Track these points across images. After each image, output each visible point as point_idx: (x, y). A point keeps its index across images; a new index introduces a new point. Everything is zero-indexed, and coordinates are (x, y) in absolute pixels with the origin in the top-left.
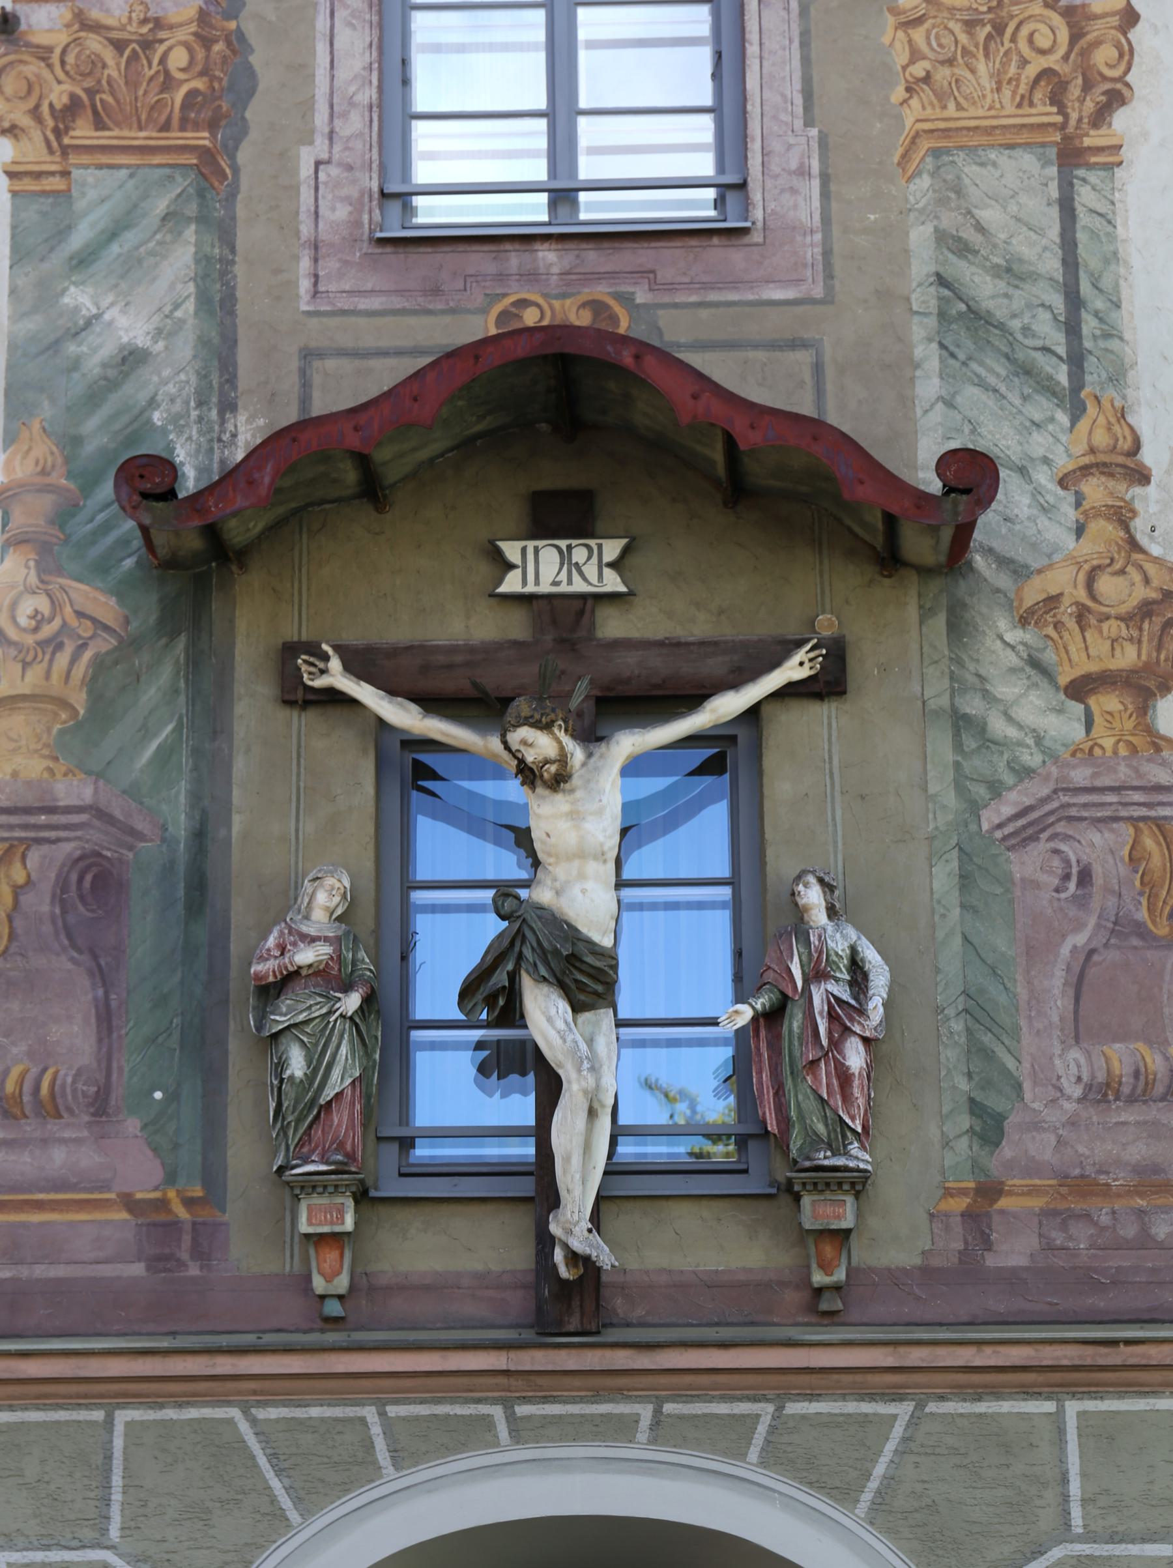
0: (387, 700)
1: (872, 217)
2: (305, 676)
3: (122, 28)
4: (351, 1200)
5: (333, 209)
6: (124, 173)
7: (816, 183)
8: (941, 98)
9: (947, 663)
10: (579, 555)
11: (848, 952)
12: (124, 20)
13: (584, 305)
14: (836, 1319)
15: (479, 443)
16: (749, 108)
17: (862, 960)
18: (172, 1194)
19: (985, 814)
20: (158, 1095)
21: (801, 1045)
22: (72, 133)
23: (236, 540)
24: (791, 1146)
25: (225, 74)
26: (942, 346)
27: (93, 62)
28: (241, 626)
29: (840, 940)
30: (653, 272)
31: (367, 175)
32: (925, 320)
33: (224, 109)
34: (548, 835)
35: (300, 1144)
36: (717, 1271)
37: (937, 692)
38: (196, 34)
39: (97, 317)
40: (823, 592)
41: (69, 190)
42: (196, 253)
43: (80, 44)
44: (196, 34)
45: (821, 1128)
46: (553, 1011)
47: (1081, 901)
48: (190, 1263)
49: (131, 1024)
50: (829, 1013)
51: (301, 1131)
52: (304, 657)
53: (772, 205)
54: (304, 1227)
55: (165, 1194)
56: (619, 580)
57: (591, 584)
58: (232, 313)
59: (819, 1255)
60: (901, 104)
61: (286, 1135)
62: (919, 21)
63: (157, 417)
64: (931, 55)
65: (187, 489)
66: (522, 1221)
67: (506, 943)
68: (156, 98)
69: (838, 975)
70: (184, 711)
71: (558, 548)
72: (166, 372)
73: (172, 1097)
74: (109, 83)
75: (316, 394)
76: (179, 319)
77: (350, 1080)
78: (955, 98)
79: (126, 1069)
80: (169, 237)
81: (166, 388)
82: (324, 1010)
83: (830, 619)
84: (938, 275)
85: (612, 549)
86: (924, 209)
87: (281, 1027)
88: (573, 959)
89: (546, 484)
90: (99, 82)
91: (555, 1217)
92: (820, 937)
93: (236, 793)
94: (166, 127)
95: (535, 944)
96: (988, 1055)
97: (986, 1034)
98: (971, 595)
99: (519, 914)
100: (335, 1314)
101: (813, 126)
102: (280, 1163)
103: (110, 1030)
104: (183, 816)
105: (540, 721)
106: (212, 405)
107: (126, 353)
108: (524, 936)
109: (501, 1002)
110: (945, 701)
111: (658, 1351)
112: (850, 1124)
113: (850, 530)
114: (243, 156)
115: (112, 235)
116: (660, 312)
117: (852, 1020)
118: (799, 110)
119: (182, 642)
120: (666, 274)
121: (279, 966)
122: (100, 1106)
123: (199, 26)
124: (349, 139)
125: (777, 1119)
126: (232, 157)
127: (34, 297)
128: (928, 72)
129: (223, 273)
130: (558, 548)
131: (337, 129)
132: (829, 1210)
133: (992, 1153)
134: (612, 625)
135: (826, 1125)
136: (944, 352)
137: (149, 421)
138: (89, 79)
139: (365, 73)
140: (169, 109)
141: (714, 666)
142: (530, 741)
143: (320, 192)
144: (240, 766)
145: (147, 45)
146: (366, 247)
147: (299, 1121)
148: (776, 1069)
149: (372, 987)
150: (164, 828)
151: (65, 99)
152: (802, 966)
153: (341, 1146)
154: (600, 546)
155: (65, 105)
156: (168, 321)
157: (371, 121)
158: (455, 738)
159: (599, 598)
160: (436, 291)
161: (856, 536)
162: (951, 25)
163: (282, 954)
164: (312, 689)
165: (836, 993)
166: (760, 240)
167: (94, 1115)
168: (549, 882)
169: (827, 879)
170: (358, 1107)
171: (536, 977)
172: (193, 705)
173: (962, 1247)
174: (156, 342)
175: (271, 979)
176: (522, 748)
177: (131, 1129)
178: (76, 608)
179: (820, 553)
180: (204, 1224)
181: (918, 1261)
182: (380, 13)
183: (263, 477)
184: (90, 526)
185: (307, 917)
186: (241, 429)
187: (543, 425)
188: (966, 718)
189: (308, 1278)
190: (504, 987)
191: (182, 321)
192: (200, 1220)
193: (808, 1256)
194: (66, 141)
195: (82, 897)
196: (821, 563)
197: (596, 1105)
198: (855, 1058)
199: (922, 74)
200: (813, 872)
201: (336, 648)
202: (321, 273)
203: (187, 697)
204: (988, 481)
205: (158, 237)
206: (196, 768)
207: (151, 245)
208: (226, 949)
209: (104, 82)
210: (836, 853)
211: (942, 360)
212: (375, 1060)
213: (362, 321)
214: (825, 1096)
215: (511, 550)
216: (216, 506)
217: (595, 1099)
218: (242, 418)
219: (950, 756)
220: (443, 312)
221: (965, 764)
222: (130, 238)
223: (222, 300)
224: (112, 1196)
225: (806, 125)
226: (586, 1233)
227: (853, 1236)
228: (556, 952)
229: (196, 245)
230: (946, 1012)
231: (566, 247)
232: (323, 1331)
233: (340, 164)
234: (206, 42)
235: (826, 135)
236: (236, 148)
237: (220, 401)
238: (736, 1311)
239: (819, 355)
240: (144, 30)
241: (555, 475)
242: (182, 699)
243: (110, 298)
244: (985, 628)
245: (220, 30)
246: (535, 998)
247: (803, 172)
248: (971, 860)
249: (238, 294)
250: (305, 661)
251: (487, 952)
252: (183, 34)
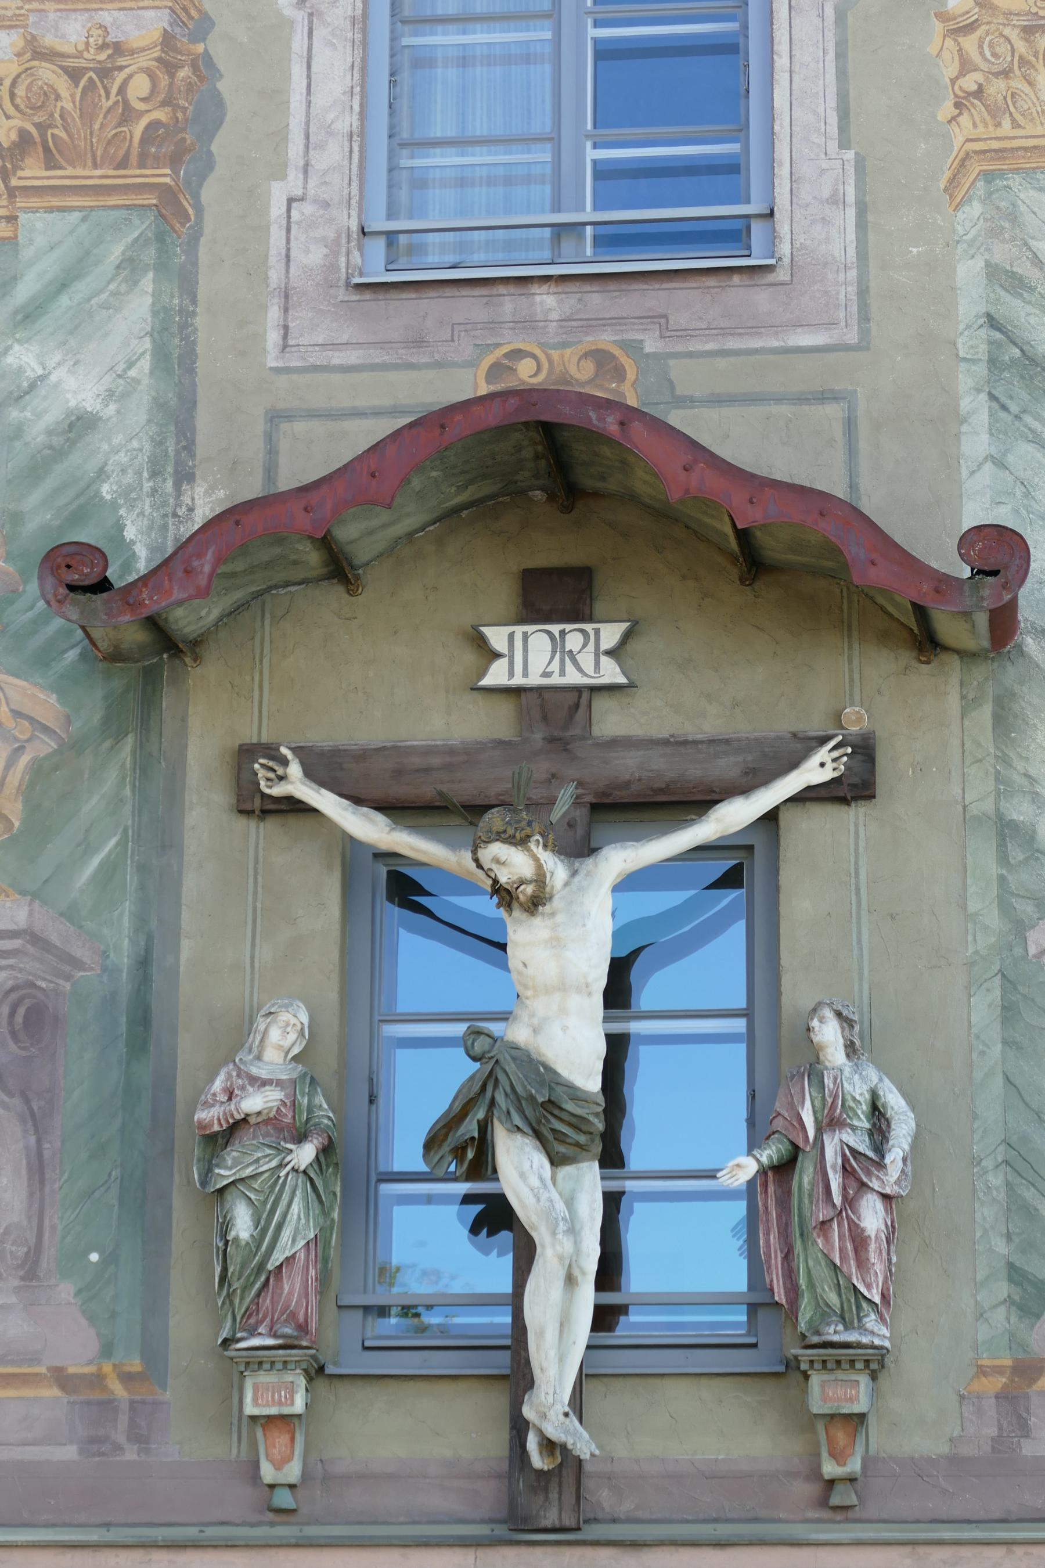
0: (350, 809)
1: (915, 250)
2: (262, 783)
3: (79, 55)
4: (302, 1378)
5: (307, 252)
6: (76, 215)
7: (851, 213)
8: (995, 113)
9: (992, 761)
10: (574, 641)
11: (868, 1096)
12: (81, 47)
13: (586, 355)
14: (850, 1514)
15: (464, 514)
16: (777, 128)
17: (883, 1106)
18: (107, 1368)
19: (1032, 936)
20: (94, 1257)
21: (811, 1202)
22: (20, 173)
23: (187, 630)
24: (800, 1318)
25: (190, 104)
26: (992, 397)
27: (45, 94)
28: (195, 724)
29: (857, 1085)
30: (665, 316)
31: (345, 212)
32: (973, 368)
33: (188, 142)
34: (525, 965)
35: (247, 1314)
36: (716, 1460)
37: (980, 795)
38: (158, 60)
39: (43, 378)
40: (852, 680)
41: (16, 237)
42: (153, 304)
43: (32, 75)
44: (158, 60)
45: (833, 1298)
46: (526, 1166)
48: (127, 1446)
49: (66, 1176)
50: (843, 1167)
51: (248, 1300)
52: (261, 761)
53: (800, 239)
54: (250, 1410)
55: (100, 1369)
56: (618, 670)
57: (586, 675)
58: (191, 371)
59: (830, 1441)
60: (949, 122)
61: (232, 1303)
62: (970, 28)
63: (106, 491)
64: (983, 66)
65: (138, 571)
66: (497, 1400)
67: (476, 1088)
68: (114, 132)
69: (856, 1123)
70: (130, 822)
71: (549, 633)
72: (118, 439)
73: (110, 1259)
74: (62, 116)
75: (283, 460)
76: (133, 379)
77: (303, 1243)
78: (1011, 114)
79: (60, 1228)
80: (123, 288)
81: (117, 457)
82: (274, 1163)
83: (858, 712)
84: (989, 315)
85: (611, 634)
86: (974, 240)
87: (225, 1182)
88: (551, 1106)
89: (541, 560)
90: (52, 115)
91: (530, 1398)
92: (835, 1079)
93: (185, 914)
94: (123, 163)
95: (508, 1089)
96: (1029, 1213)
97: (1028, 1189)
98: (1021, 683)
99: (492, 1054)
100: (284, 1506)
101: (849, 148)
102: (224, 1335)
103: (42, 1181)
104: (126, 942)
105: (514, 836)
106: (167, 476)
107: (73, 418)
108: (497, 1079)
109: (470, 1154)
110: (988, 806)
111: (646, 1549)
112: (866, 1293)
113: (883, 609)
115: (61, 286)
116: (671, 362)
117: (869, 1174)
118: (833, 129)
119: (129, 743)
120: (679, 319)
121: (225, 1113)
123: (162, 51)
124: (325, 173)
125: (785, 1288)
126: (196, 196)
128: (980, 86)
129: (183, 326)
130: (549, 633)
131: (313, 162)
132: (840, 1392)
133: (1033, 1326)
134: (610, 721)
135: (840, 1295)
136: (995, 405)
137: (97, 494)
138: (41, 113)
139: (346, 98)
140: (127, 144)
141: (725, 767)
142: (503, 859)
143: (293, 232)
144: (191, 884)
145: (105, 72)
146: (342, 294)
147: (245, 1289)
148: (786, 1230)
149: (330, 1137)
150: (105, 955)
151: (14, 136)
152: (815, 1113)
153: (293, 1315)
154: (597, 631)
155: (13, 143)
156: (121, 381)
157: (351, 152)
158: (425, 853)
159: (595, 689)
160: (418, 343)
161: (890, 615)
162: (1007, 31)
163: (230, 1099)
164: (270, 797)
165: (852, 1144)
166: (788, 278)
167: (23, 1279)
168: (526, 1019)
169: (845, 1013)
170: (312, 1272)
171: (509, 1126)
172: (139, 816)
173: (996, 1434)
174: (107, 406)
175: (216, 1128)
176: (494, 867)
177: (63, 1295)
178: (13, 707)
179: (850, 636)
180: (143, 1402)
181: (944, 1449)
182: (364, 31)
183: (203, 565)
184: (30, 614)
185: (259, 1058)
186: (199, 502)
187: (537, 492)
188: (1013, 825)
189: (256, 1465)
190: (473, 1138)
191: (137, 381)
192: (138, 1398)
193: (817, 1445)
194: (14, 182)
195: (14, 1034)
196: (850, 647)
197: (576, 1272)
198: (872, 1217)
199: (975, 87)
200: (830, 1005)
201: (296, 750)
202: (291, 325)
203: (134, 806)
204: (1017, 562)
205: (112, 287)
206: (142, 887)
207: (104, 296)
208: (171, 1092)
209: (57, 116)
210: (861, 980)
211: (992, 414)
212: (333, 1220)
213: (336, 378)
214: (838, 1262)
215: (497, 637)
216: (151, 598)
217: (574, 1265)
218: (200, 490)
219: (993, 869)
220: (427, 366)
221: (1010, 878)
222: (81, 289)
223: (180, 357)
224: (43, 1370)
225: (841, 146)
226: (562, 1417)
227: (871, 1420)
228: (532, 1098)
229: (153, 295)
230: (984, 1163)
231: (568, 290)
232: (272, 1524)
233: (315, 201)
234: (170, 68)
235: (864, 159)
236: (200, 186)
237: (176, 472)
239: (852, 409)
240: (102, 57)
241: (550, 552)
242: (128, 808)
243: (58, 357)
244: (1036, 721)
245: (185, 56)
246: (508, 1151)
247: (836, 200)
248: (1015, 989)
249: (199, 349)
250: (262, 765)
251: (455, 1098)
252: (144, 61)
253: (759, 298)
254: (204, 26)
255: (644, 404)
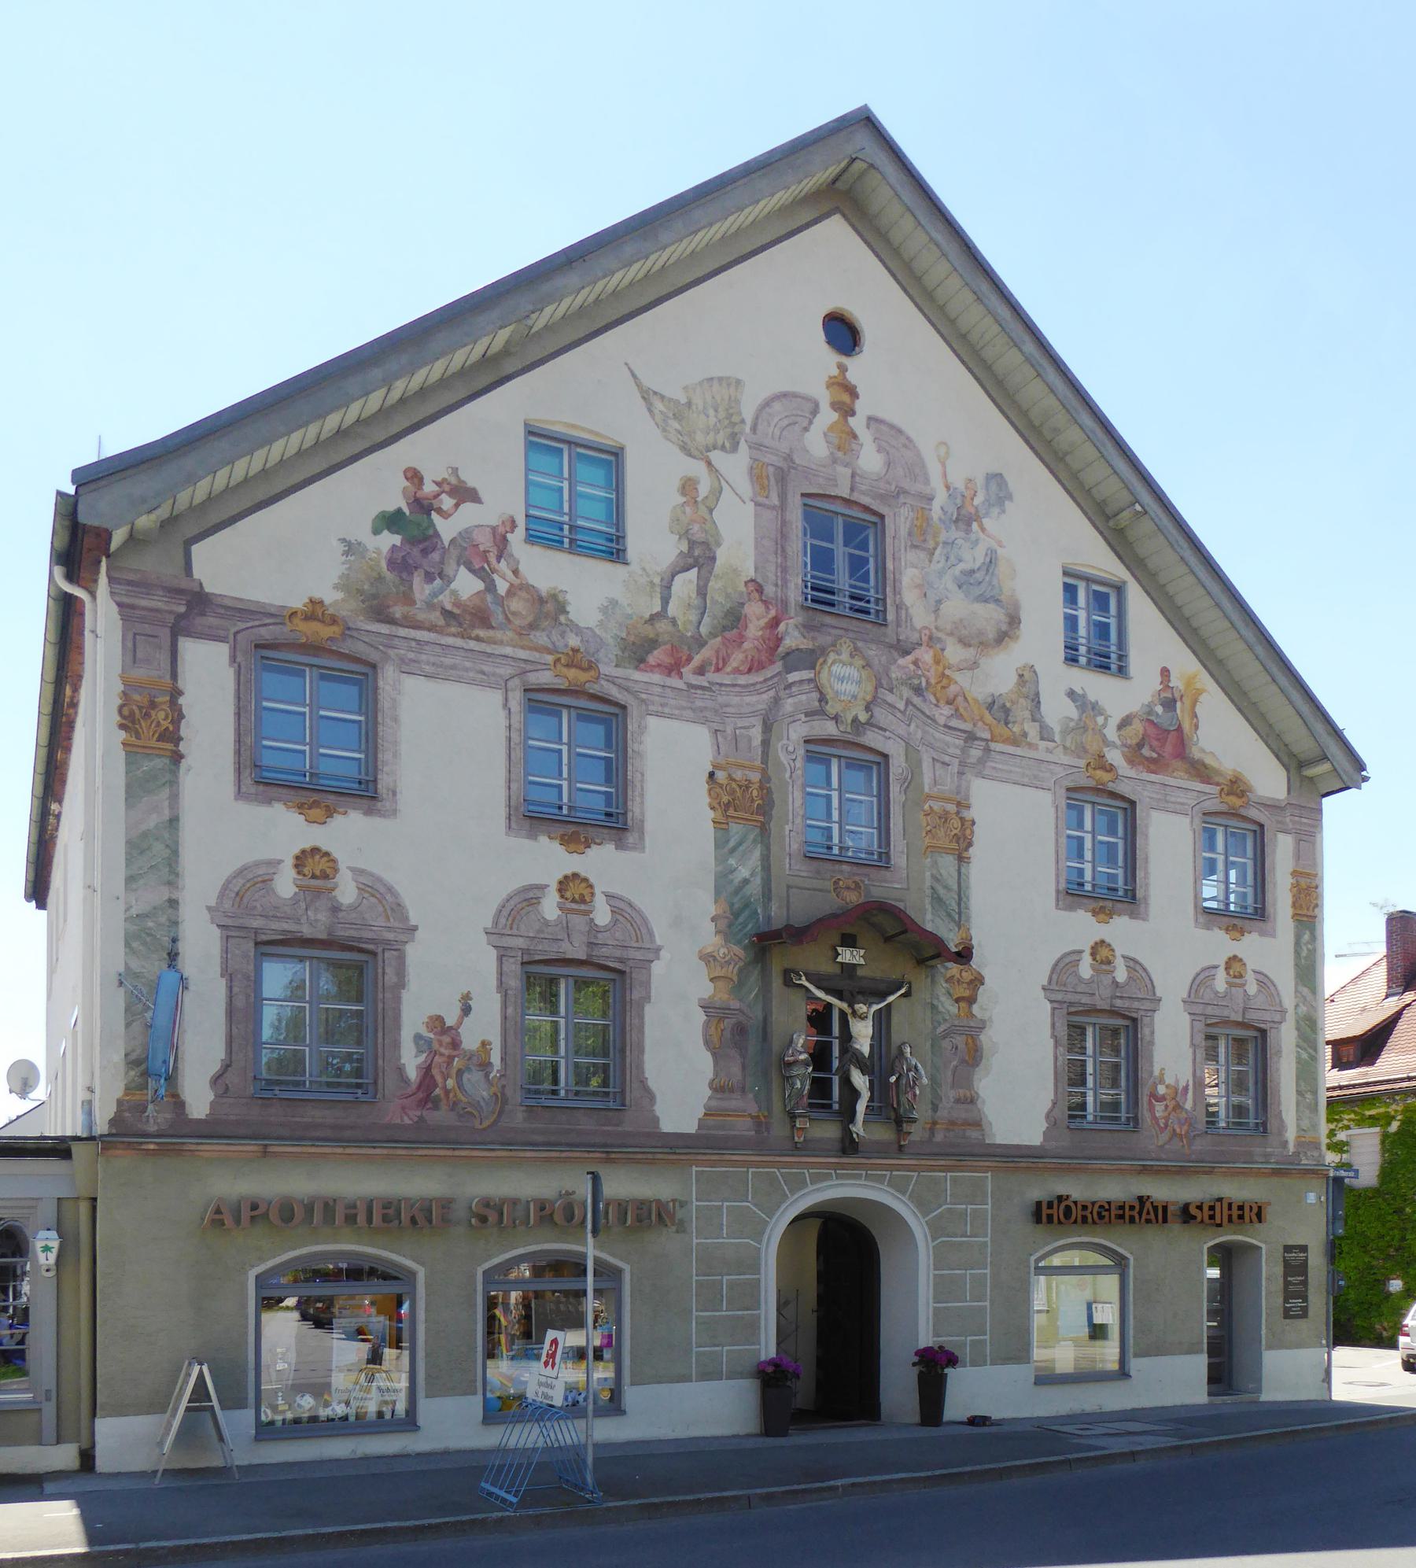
47: (955, 1054)
114: (772, 824)
115: (740, 844)
122: (743, 1090)
127: (720, 859)
134: (860, 972)
215: (839, 949)
222: (744, 846)
231: (97, 989)
238: (880, 1150)
253: (888, 874)
254: (769, 780)
255: (66, 846)
